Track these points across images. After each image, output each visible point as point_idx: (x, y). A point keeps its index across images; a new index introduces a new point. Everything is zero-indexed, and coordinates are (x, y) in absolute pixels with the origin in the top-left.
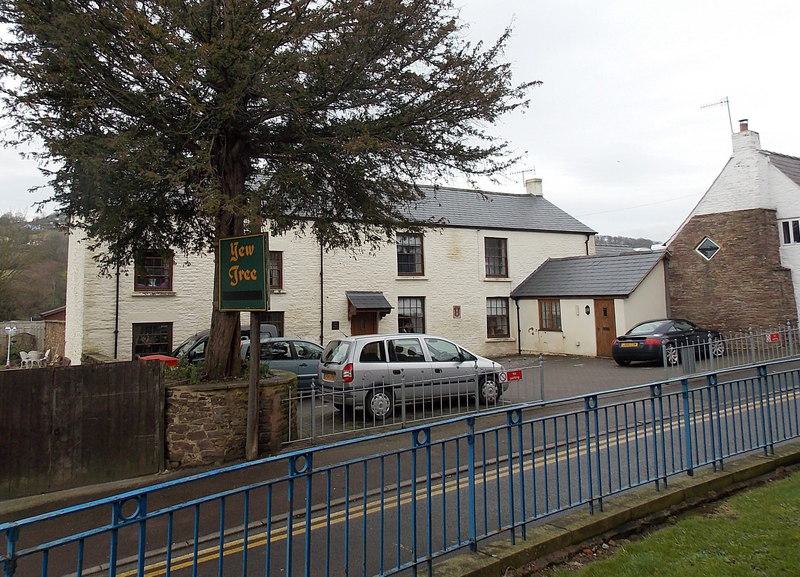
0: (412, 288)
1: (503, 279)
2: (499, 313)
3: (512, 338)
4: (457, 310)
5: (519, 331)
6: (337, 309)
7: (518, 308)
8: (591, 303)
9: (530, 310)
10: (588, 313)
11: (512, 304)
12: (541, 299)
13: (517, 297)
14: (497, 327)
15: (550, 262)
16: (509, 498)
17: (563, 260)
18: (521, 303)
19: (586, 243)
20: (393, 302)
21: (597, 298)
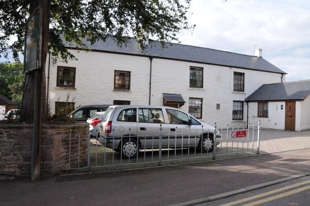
0: (196, 93)
1: (242, 92)
2: (239, 109)
3: (244, 121)
4: (218, 106)
5: (248, 117)
6: (157, 102)
7: (248, 107)
8: (284, 103)
9: (254, 107)
10: (282, 109)
11: (245, 104)
12: (259, 102)
13: (248, 101)
14: (238, 114)
15: (264, 86)
16: (50, 62)
17: (250, 56)
18: (250, 104)
19: (282, 78)
20: (186, 99)
21: (287, 101)
